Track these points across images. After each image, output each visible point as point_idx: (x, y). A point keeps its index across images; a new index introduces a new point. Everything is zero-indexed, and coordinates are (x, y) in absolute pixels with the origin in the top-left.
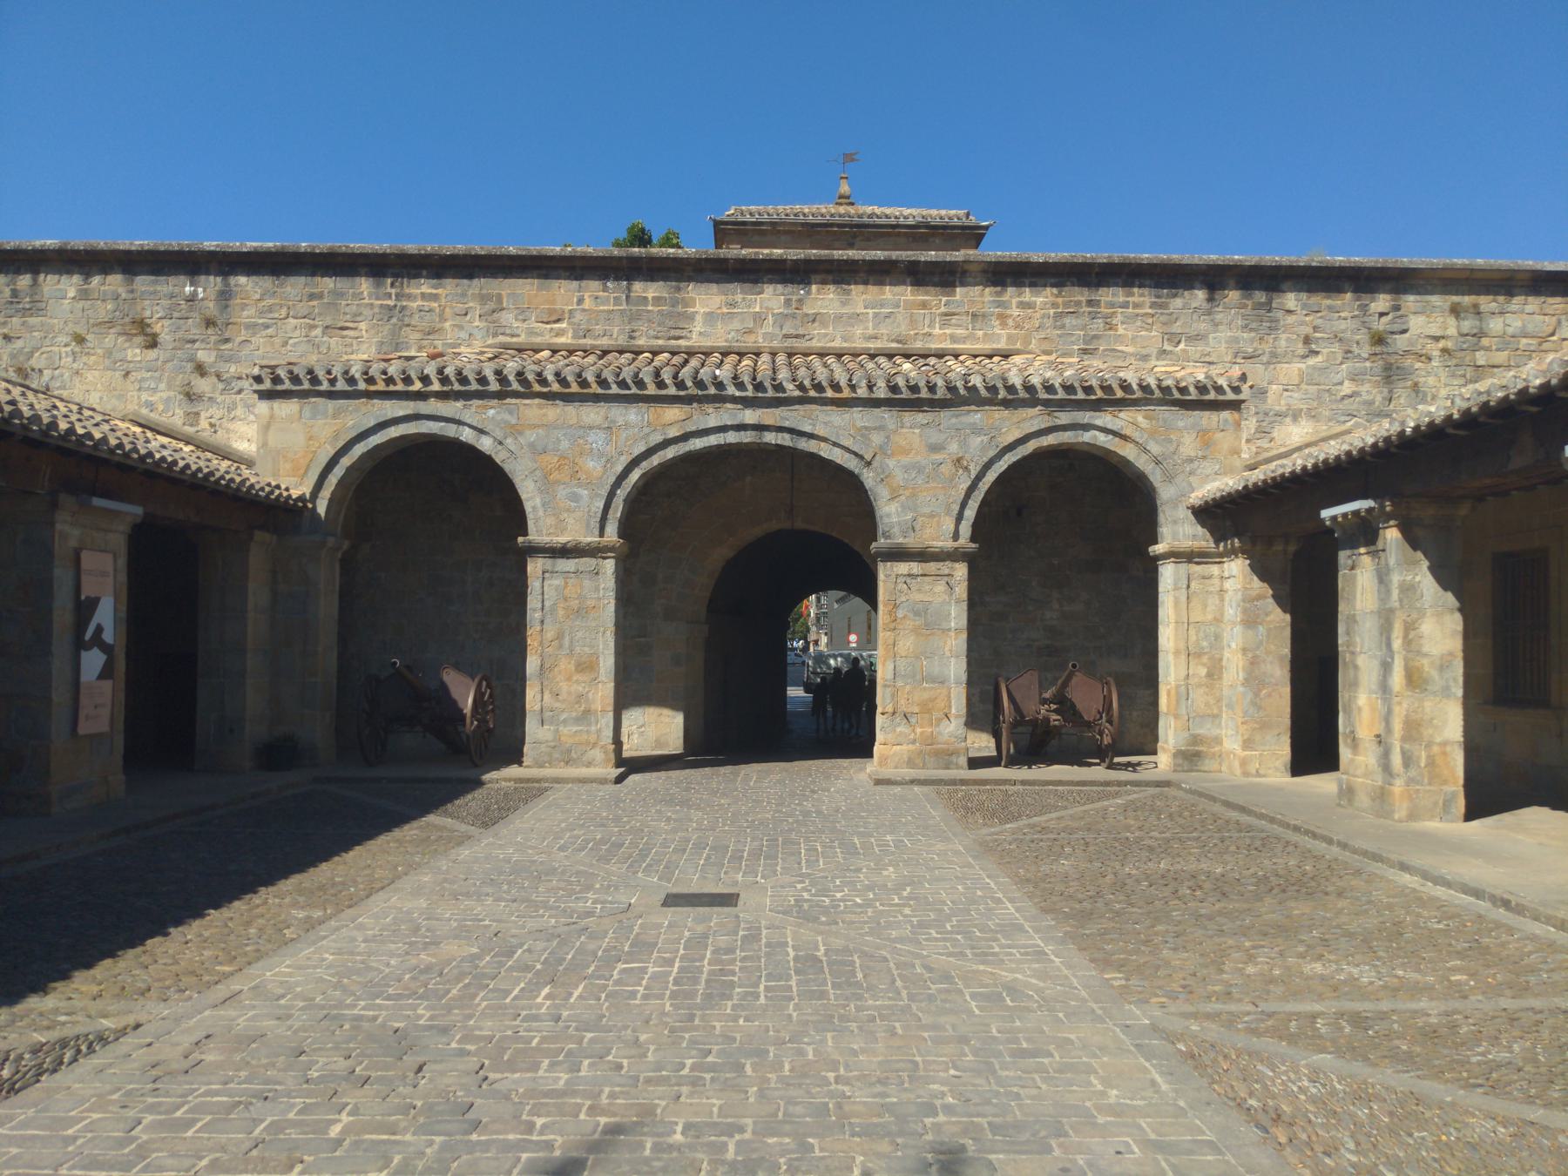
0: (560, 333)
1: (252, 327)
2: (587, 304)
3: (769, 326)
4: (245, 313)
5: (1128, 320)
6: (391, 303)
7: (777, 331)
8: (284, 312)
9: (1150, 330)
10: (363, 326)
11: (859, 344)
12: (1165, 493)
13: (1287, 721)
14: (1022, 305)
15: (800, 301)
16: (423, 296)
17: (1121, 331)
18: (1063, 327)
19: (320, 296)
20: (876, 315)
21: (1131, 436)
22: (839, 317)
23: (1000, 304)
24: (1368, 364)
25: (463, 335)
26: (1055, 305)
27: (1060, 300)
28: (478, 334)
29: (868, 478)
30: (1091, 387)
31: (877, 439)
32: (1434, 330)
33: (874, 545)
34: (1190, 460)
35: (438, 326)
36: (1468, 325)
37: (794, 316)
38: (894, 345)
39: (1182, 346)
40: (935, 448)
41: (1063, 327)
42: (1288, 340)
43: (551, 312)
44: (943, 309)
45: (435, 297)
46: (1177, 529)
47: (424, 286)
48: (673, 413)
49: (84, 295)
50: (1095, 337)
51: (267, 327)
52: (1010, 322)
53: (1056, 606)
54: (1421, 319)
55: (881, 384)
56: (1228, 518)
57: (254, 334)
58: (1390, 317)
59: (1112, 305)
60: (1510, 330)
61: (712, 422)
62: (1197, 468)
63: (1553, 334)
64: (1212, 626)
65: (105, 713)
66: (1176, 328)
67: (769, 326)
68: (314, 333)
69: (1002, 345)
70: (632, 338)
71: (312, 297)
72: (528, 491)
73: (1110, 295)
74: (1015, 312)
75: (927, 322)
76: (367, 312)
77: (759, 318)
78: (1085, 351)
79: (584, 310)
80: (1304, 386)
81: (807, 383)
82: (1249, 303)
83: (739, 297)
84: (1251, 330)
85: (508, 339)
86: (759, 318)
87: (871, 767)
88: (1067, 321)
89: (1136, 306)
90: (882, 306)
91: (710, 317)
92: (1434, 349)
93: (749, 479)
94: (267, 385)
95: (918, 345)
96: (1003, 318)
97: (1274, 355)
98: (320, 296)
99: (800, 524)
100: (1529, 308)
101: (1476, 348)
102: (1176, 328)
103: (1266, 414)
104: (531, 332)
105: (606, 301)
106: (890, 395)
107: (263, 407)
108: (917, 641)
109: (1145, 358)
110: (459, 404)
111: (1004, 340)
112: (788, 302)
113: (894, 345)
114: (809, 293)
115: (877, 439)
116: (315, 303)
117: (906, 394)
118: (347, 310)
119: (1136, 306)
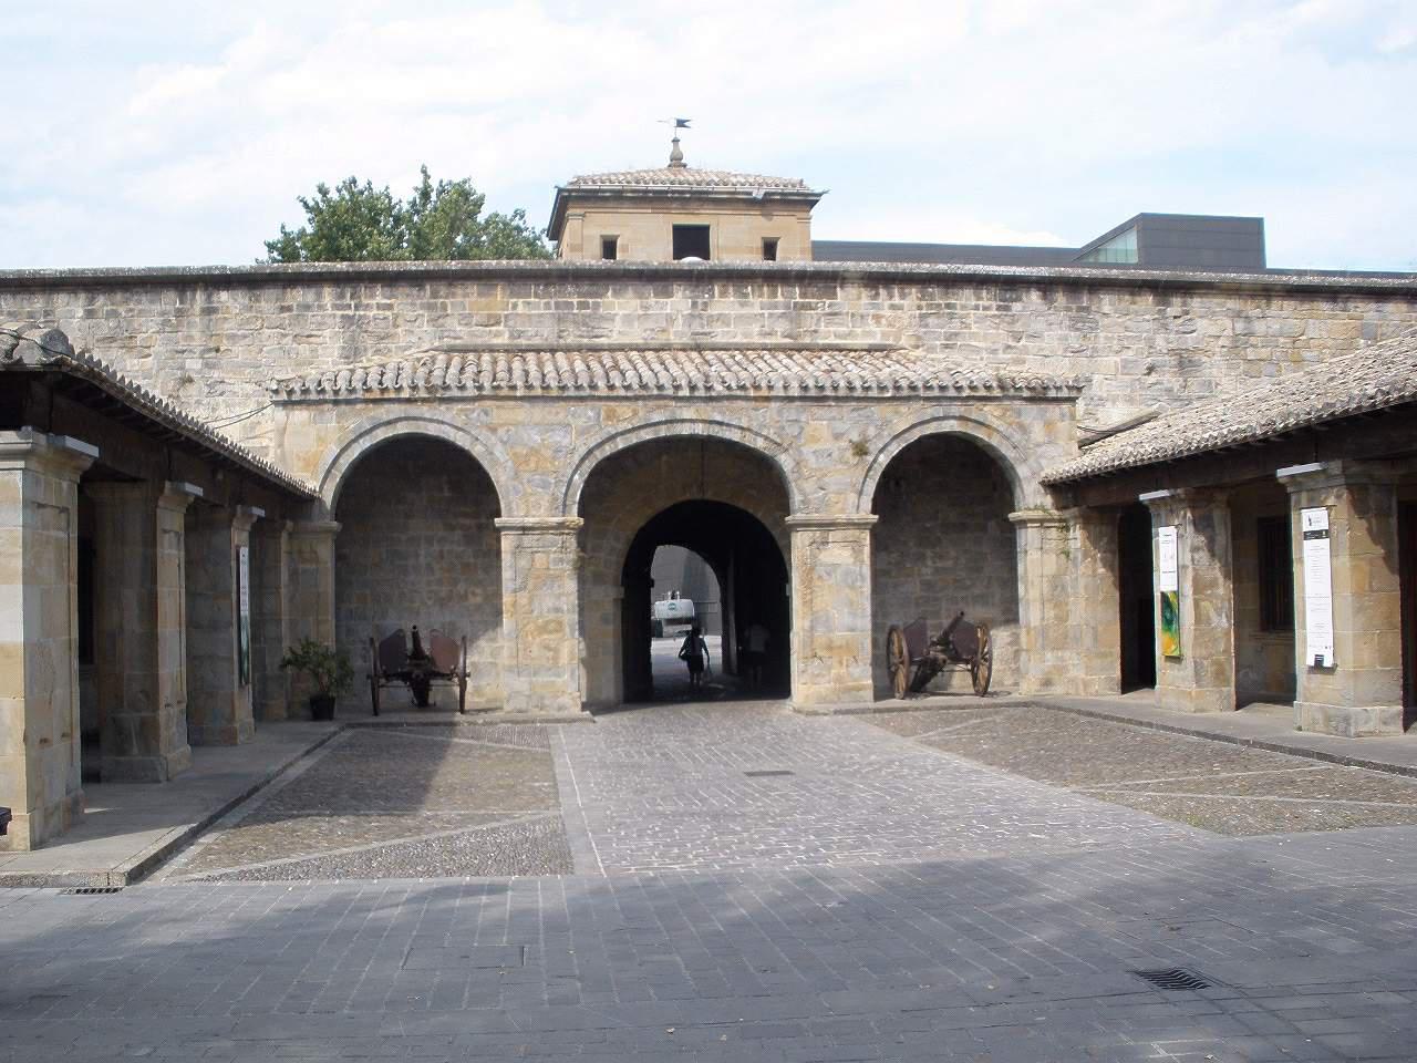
0: (498, 334)
1: (232, 337)
2: (520, 309)
3: (679, 326)
4: (226, 326)
5: (979, 320)
6: (351, 313)
7: (686, 329)
8: (259, 323)
9: (998, 328)
10: (327, 333)
11: (758, 340)
12: (1022, 471)
13: (1119, 643)
14: (893, 307)
15: (705, 304)
16: (379, 307)
17: (974, 329)
18: (927, 326)
19: (289, 309)
20: (771, 315)
21: (996, 427)
22: (740, 317)
23: (874, 306)
24: (1167, 358)
25: (414, 339)
26: (919, 308)
27: (924, 303)
28: (427, 338)
29: (785, 462)
30: (961, 387)
31: (793, 430)
32: (1214, 331)
33: (787, 519)
34: (1038, 445)
35: (392, 331)
36: (1240, 326)
37: (700, 317)
38: (787, 341)
39: (1023, 342)
40: (837, 437)
41: (927, 326)
42: (1106, 338)
43: (489, 316)
44: (827, 310)
45: (390, 307)
46: (1031, 499)
47: (379, 296)
48: (624, 410)
49: (90, 314)
50: (956, 334)
51: (245, 337)
52: (884, 321)
53: (929, 563)
54: (1205, 322)
55: (795, 384)
56: (1068, 490)
57: (233, 344)
58: (1181, 320)
59: (964, 307)
60: (1270, 331)
61: (656, 418)
62: (1042, 454)
63: (1302, 335)
64: (1058, 570)
65: (1161, 538)
66: (1018, 327)
67: (679, 326)
68: (285, 341)
69: (877, 340)
70: (560, 337)
71: (283, 309)
72: (500, 477)
73: (965, 298)
74: (887, 312)
75: (815, 320)
76: (330, 321)
77: (670, 319)
78: (947, 346)
79: (517, 314)
80: (1120, 376)
81: (734, 385)
82: (1074, 306)
83: (652, 300)
84: (1077, 329)
85: (453, 342)
86: (670, 319)
87: (785, 708)
88: (930, 320)
89: (985, 308)
90: (776, 308)
91: (628, 319)
92: (1216, 346)
93: (664, 458)
94: (284, 397)
95: (807, 340)
96: (877, 318)
97: (1095, 349)
98: (289, 309)
99: (709, 496)
100: (1284, 314)
101: (1247, 345)
102: (1018, 327)
103: (1092, 399)
104: (472, 334)
105: (537, 306)
106: (803, 394)
107: (280, 414)
108: (832, 593)
109: (994, 351)
110: (443, 407)
111: (879, 336)
112: (694, 304)
113: (787, 341)
114: (713, 296)
115: (793, 430)
116: (286, 315)
117: (813, 393)
118: (314, 320)
119: (985, 308)
